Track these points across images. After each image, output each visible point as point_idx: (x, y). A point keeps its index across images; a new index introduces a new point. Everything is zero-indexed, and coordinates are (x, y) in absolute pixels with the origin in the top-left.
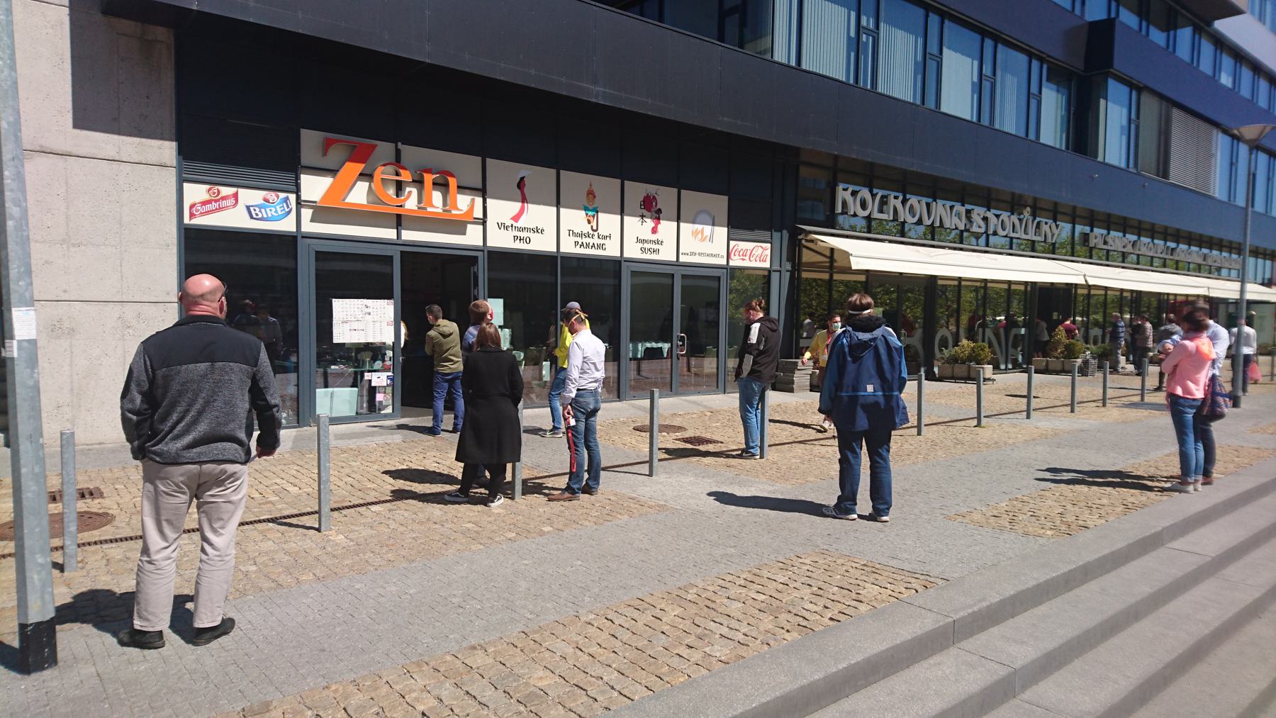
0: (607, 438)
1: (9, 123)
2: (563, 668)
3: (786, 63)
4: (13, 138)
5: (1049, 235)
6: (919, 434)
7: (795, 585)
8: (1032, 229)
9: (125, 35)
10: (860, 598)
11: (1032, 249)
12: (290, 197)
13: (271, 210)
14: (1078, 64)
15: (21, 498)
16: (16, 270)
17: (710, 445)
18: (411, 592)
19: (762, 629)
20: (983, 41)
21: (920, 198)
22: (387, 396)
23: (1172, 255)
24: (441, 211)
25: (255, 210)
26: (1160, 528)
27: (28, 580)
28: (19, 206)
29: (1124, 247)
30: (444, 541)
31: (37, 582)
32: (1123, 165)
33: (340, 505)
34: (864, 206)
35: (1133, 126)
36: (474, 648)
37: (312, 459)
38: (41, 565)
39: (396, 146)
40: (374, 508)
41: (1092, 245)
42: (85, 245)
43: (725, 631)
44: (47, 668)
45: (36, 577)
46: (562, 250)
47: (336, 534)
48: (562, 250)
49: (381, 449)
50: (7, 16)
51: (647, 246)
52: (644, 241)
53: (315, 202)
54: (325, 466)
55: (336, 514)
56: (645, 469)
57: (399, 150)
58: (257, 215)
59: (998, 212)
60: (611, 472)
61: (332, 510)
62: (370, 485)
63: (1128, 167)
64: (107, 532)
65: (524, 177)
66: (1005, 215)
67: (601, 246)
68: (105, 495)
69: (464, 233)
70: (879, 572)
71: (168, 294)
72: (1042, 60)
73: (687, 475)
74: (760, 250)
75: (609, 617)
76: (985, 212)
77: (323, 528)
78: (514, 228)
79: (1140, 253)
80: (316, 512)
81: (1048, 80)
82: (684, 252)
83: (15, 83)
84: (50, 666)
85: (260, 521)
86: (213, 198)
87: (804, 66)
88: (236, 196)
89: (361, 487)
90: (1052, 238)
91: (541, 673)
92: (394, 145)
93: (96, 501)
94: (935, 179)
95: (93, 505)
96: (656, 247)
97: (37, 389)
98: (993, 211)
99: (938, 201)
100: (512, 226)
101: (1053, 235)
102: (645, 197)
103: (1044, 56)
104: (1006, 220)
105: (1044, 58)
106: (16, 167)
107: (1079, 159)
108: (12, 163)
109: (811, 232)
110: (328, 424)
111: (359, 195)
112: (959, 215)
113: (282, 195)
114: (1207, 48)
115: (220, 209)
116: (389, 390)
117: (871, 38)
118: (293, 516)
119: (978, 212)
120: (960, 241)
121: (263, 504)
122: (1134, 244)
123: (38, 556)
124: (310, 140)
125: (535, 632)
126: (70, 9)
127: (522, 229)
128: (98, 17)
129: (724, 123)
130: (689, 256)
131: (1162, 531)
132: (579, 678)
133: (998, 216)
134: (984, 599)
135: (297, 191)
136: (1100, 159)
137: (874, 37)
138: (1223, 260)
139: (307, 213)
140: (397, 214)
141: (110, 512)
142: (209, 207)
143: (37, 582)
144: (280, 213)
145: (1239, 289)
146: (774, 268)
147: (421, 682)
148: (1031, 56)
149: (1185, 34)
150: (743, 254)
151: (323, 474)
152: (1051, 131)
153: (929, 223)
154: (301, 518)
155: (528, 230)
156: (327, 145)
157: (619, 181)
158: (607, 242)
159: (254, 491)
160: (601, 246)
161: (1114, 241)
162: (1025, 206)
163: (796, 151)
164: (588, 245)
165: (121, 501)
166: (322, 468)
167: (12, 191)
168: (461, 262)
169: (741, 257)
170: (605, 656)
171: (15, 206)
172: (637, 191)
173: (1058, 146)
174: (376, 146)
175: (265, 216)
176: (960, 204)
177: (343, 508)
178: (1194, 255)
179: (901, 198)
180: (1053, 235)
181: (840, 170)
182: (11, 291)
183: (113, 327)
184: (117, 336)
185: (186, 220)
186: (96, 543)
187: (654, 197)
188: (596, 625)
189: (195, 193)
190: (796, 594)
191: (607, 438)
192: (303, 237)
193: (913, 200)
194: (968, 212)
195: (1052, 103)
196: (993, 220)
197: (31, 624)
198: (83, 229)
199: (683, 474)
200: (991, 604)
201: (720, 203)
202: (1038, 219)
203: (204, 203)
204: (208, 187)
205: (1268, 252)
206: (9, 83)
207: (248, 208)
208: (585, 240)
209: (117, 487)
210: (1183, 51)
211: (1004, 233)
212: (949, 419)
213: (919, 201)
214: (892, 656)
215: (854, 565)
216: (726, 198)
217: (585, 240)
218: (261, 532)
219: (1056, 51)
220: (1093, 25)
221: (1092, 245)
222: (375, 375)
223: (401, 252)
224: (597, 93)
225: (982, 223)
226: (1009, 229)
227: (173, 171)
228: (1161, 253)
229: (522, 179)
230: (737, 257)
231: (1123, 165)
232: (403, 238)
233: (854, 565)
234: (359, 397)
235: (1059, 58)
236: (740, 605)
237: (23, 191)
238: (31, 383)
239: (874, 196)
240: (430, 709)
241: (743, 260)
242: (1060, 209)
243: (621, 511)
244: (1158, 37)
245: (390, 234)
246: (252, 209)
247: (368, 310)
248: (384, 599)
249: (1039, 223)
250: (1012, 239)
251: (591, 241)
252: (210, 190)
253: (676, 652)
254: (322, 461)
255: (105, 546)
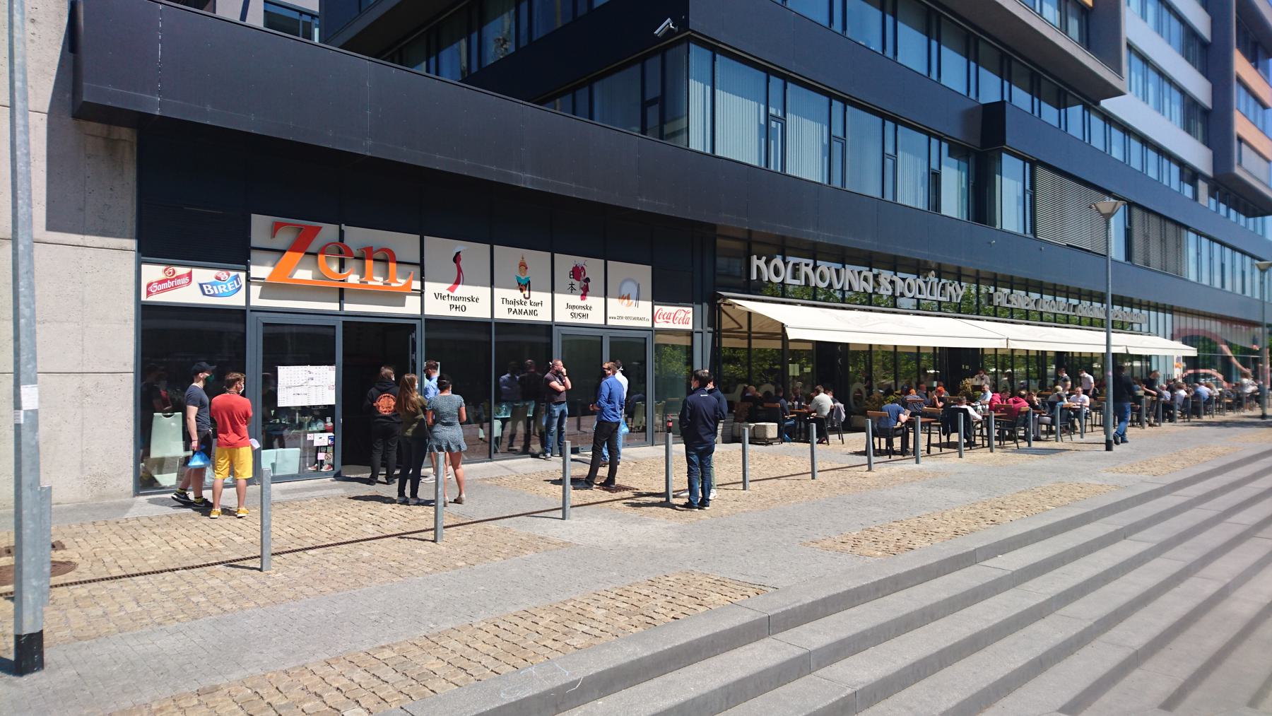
0: (533, 488)
1: (25, 246)
2: (451, 657)
3: (703, 151)
4: (27, 257)
5: (954, 295)
6: (813, 478)
7: (655, 596)
8: (937, 291)
9: (92, 136)
10: (703, 603)
11: (940, 309)
12: (240, 276)
13: (222, 287)
14: (975, 142)
15: (21, 533)
16: (25, 357)
17: (626, 492)
18: (337, 612)
19: (616, 626)
20: (884, 125)
21: (830, 264)
22: (329, 455)
23: (1074, 311)
24: (382, 284)
25: (207, 287)
26: (974, 548)
27: (24, 600)
28: (30, 307)
29: (1027, 305)
30: (369, 575)
31: (31, 601)
32: (1021, 232)
33: (280, 551)
34: (777, 273)
35: (1028, 196)
36: (383, 647)
37: (256, 513)
38: (35, 588)
39: (340, 228)
40: (311, 552)
41: (996, 303)
42: (49, 322)
43: (586, 628)
44: (36, 671)
45: (30, 596)
46: (496, 316)
47: (277, 571)
48: (496, 316)
49: (320, 503)
50: (27, 167)
51: (576, 311)
52: (574, 307)
53: (263, 279)
54: (267, 514)
55: (276, 558)
56: (559, 514)
57: (343, 231)
58: (209, 291)
59: (904, 275)
60: (539, 519)
61: (273, 554)
62: (308, 534)
63: (1025, 233)
64: (70, 577)
65: (459, 252)
66: (911, 278)
67: (533, 312)
68: (66, 547)
69: (403, 305)
70: (725, 584)
71: (125, 365)
72: (940, 139)
73: (597, 518)
74: (683, 314)
75: (496, 624)
76: (892, 276)
77: (264, 568)
78: (450, 298)
79: (1042, 310)
80: (259, 557)
81: (950, 155)
82: (611, 316)
83: (31, 216)
84: (38, 670)
85: (208, 565)
86: (168, 277)
87: (718, 153)
88: (190, 275)
89: (300, 535)
90: (957, 300)
91: (434, 661)
92: (338, 226)
93: (59, 552)
94: (844, 249)
95: (58, 556)
96: (585, 312)
97: (37, 447)
98: (900, 274)
99: (847, 266)
100: (448, 296)
101: (957, 296)
102: (574, 268)
103: (942, 135)
104: (912, 283)
105: (942, 137)
106: (29, 279)
107: (979, 228)
108: (26, 275)
109: (729, 297)
110: (270, 482)
111: (304, 275)
112: (866, 279)
113: (233, 274)
114: (1097, 123)
115: (175, 287)
116: (330, 449)
117: (779, 124)
118: (238, 560)
119: (886, 275)
120: (869, 302)
121: (212, 551)
122: (1036, 302)
123: (33, 580)
124: (260, 225)
125: (434, 636)
126: (48, 116)
127: (459, 299)
128: (69, 120)
129: (643, 203)
130: (616, 320)
131: (975, 550)
132: (464, 663)
133: (904, 280)
134: (799, 601)
135: (247, 271)
136: (998, 227)
137: (782, 124)
138: (1125, 314)
139: (255, 290)
140: (340, 288)
141: (72, 560)
142: (164, 285)
143: (31, 601)
144: (231, 289)
145: (1105, 343)
146: (696, 330)
147: (338, 670)
148: (930, 135)
149: (1076, 112)
150: (667, 317)
151: (265, 521)
152: (953, 203)
153: (839, 287)
154: (246, 561)
155: (464, 299)
156: (276, 228)
157: (549, 254)
158: (539, 308)
159: (203, 541)
160: (533, 312)
161: (1017, 300)
162: (930, 270)
163: (713, 227)
164: (520, 312)
165: (81, 552)
166: (264, 515)
167: (25, 296)
168: (400, 330)
169: (666, 320)
170: (485, 648)
171: (27, 308)
172: (566, 262)
173: (960, 218)
174: (320, 228)
175: (217, 292)
176: (868, 269)
177: (283, 553)
178: (1096, 310)
179: (811, 265)
180: (957, 296)
181: (753, 244)
182: (21, 373)
183: (73, 396)
184: (77, 404)
185: (144, 298)
186: (62, 585)
187: (583, 268)
188: (484, 629)
189: (152, 272)
190: (653, 602)
191: (533, 488)
192: (252, 311)
193: (823, 266)
194: (876, 277)
195: (953, 180)
196: (899, 282)
197: (25, 635)
198: (48, 308)
199: (593, 517)
200: (804, 605)
201: (644, 273)
202: (943, 281)
203: (160, 282)
204: (163, 267)
205: (1160, 306)
206: (27, 216)
207: (201, 285)
208: (518, 307)
209: (77, 540)
210: (1075, 129)
211: (911, 295)
212: (848, 465)
213: (828, 268)
214: (712, 641)
215: (708, 580)
216: (649, 268)
217: (518, 307)
218: (209, 574)
219: (955, 132)
220: (987, 107)
221: (996, 303)
222: (317, 436)
223: (343, 322)
224: (526, 179)
225: (889, 287)
226: (916, 291)
227: (133, 255)
228: (1063, 310)
229: (458, 254)
230: (662, 320)
231: (1021, 232)
232: (345, 309)
233: (708, 580)
234: (302, 459)
235: (961, 139)
236: (604, 611)
237: (33, 296)
238: (33, 443)
239: (786, 264)
240: (343, 686)
241: (667, 322)
242: (963, 272)
243: (528, 548)
244: (1049, 114)
245: (335, 307)
246: (204, 286)
247: (311, 376)
248: (314, 618)
249: (944, 285)
250: (918, 300)
251: (523, 308)
252: (166, 270)
253: (544, 643)
254: (264, 510)
255: (71, 587)
